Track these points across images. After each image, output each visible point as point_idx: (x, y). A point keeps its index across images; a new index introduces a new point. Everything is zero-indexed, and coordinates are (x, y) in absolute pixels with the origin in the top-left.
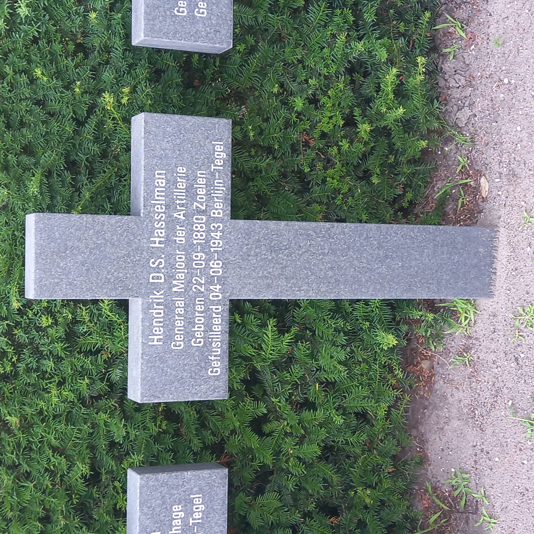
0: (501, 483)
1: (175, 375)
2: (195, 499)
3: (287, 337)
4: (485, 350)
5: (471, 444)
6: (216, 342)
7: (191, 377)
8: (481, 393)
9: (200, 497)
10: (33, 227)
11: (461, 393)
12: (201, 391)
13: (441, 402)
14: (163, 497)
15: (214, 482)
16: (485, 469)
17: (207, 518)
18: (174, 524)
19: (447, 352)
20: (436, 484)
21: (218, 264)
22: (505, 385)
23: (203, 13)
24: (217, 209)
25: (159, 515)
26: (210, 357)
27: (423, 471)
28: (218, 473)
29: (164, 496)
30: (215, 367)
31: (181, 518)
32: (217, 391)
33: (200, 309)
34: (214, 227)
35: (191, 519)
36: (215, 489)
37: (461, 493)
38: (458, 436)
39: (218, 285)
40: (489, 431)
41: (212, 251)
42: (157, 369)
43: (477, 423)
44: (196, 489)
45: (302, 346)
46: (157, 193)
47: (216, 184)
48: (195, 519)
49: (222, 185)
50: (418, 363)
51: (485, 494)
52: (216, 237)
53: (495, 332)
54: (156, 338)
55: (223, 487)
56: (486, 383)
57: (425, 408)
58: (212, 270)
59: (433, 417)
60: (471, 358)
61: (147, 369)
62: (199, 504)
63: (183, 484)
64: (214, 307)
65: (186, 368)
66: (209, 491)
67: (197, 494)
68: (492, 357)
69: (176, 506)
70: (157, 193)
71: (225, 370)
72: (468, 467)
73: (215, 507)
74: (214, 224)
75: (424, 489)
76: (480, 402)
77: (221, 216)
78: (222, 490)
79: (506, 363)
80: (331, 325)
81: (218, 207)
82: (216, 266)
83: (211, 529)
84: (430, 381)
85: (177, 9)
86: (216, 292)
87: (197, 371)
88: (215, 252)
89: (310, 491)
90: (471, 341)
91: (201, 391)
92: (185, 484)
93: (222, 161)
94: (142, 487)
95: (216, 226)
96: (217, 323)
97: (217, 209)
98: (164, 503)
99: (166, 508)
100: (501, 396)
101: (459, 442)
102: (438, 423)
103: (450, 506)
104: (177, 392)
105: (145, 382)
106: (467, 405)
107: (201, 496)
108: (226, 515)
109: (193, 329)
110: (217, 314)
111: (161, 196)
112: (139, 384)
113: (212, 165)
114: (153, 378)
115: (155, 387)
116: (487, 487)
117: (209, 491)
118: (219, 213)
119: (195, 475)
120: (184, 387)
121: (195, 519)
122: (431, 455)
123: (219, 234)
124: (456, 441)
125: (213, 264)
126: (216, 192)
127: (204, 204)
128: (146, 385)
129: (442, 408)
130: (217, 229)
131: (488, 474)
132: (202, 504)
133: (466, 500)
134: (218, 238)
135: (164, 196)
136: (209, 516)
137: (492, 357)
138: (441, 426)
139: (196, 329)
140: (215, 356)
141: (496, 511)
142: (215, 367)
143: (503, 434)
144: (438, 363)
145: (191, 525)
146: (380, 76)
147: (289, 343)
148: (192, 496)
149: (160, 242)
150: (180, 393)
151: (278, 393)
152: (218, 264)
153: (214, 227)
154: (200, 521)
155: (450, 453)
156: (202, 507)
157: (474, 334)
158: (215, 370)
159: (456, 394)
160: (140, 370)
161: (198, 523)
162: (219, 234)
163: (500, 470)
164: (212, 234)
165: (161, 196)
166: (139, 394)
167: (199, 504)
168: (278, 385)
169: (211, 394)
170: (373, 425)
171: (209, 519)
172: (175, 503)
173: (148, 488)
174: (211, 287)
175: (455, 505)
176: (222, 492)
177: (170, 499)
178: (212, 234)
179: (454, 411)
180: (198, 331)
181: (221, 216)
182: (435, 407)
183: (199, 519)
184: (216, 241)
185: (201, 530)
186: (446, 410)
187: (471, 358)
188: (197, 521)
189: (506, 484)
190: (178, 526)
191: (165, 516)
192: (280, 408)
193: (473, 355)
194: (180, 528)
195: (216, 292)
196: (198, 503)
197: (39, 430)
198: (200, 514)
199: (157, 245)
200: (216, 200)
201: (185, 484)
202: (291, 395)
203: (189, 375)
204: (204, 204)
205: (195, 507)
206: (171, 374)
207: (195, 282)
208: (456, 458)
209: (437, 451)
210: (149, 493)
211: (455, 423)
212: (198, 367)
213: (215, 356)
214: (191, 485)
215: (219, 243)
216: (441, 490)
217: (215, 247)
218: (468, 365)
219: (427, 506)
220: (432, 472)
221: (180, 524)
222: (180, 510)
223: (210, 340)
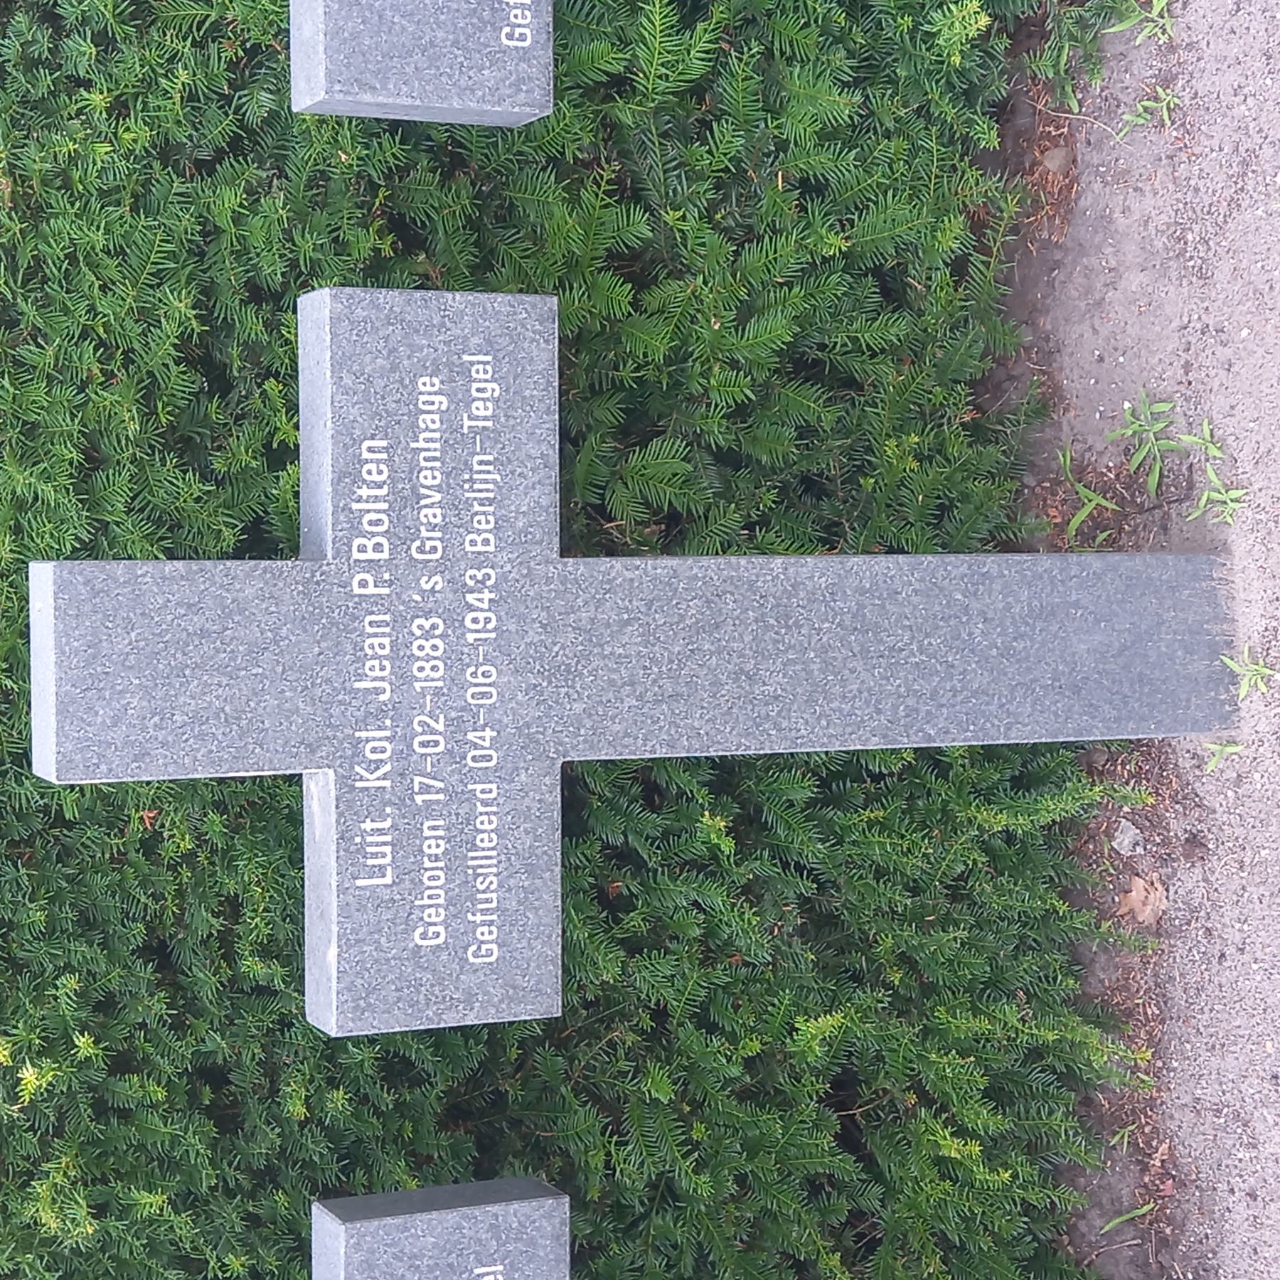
0: (1255, 394)
1: (413, 33)
2: (476, 367)
3: (701, 37)
4: (1211, 66)
5: (1176, 323)
6: (486, 875)
7: (455, 43)
8: (1201, 184)
9: (488, 363)
10: (50, 657)
11: (1149, 201)
12: (483, 86)
13: (1096, 232)
14: (390, 352)
15: (523, 326)
16: (1212, 373)
17: (507, 417)
18: (423, 426)
19: (1111, 106)
20: (1083, 456)
22: (1266, 138)
24: (479, 532)
25: (383, 398)
27: (1049, 433)
28: (534, 306)
29: (395, 350)
30: (519, 26)
31: (439, 411)
32: (524, 88)
33: (434, 851)
35: (465, 416)
36: (526, 345)
37: (1149, 461)
38: (1141, 314)
40: (1222, 273)
42: (367, 14)
43: (1191, 263)
44: (475, 340)
45: (741, 60)
48: (477, 418)
50: (1035, 163)
51: (1212, 436)
52: (477, 604)
53: (1238, 10)
55: (547, 341)
56: (1214, 154)
57: (1057, 265)
59: (1078, 279)
60: (1176, 100)
61: (340, 10)
62: (486, 381)
63: (443, 325)
64: (479, 787)
65: (443, 17)
66: (511, 348)
67: (480, 353)
68: (1233, 77)
69: (427, 379)
71: (545, 36)
72: (1167, 387)
73: (527, 393)
75: (1050, 480)
76: (1198, 209)
77: (491, 548)
78: (544, 350)
79: (1268, 82)
80: (815, 9)
81: (484, 526)
82: (481, 680)
83: (518, 448)
84: (1065, 203)
86: (483, 748)
87: (470, 29)
89: (764, 459)
90: (1173, 59)
91: (483, 86)
92: (448, 324)
94: (335, 320)
96: (486, 827)
97: (479, 532)
98: (394, 368)
99: (401, 381)
100: (1253, 172)
101: (1142, 328)
102: (1088, 291)
103: (1121, 502)
104: (420, 80)
105: (336, 43)
106: (1164, 227)
107: (489, 358)
108: (557, 417)
112: (321, 48)
114: (355, 36)
115: (361, 59)
116: (1218, 418)
117: (511, 348)
119: (474, 305)
120: (438, 68)
121: (477, 418)
122: (1073, 381)
123: (487, 595)
124: (1137, 327)
126: (476, 486)
128: (339, 51)
129: (1099, 249)
131: (1222, 384)
132: (494, 380)
133: (1161, 475)
136: (511, 413)
137: (1233, 77)
138: (1097, 297)
139: (426, 902)
141: (1240, 470)
142: (519, 26)
143: (1259, 265)
144: (1089, 143)
145: (465, 431)
147: (707, 52)
148: (466, 358)
150: (428, 83)
151: (679, 198)
154: (489, 424)
155: (1121, 359)
156: (494, 389)
157: (1184, 35)
158: (518, 31)
159: (1135, 206)
160: (321, 11)
161: (484, 428)
162: (487, 595)
163: (1252, 360)
164: (470, 598)
166: (322, 74)
167: (486, 381)
168: (679, 176)
169: (509, 97)
170: (921, 313)
171: (512, 422)
172: (423, 370)
173: (351, 323)
174: (471, 736)
175: (1133, 496)
176: (545, 356)
177: (409, 357)
178: (470, 598)
179: (1131, 251)
180: (430, 906)
182: (1082, 249)
183: (485, 418)
184: (481, 616)
185: (492, 448)
186: (1111, 249)
187: (1176, 100)
188: (481, 424)
189: (1269, 391)
190: (434, 431)
191: (398, 402)
192: (684, 238)
193: (1180, 94)
194: (437, 435)
195: (483, 748)
196: (481, 376)
197: (63, 225)
198: (489, 404)
200: (477, 508)
201: (448, 324)
202: (713, 207)
203: (451, 37)
205: (475, 385)
206: (404, 29)
208: (1136, 371)
209: (1086, 366)
210: (355, 338)
211: (1134, 281)
212: (475, 20)
214: (463, 330)
215: (488, 620)
216: (1095, 469)
217: (477, 631)
218: (1168, 123)
219: (1058, 520)
220: (1072, 429)
221: (437, 425)
222: (436, 389)
223: (470, 871)
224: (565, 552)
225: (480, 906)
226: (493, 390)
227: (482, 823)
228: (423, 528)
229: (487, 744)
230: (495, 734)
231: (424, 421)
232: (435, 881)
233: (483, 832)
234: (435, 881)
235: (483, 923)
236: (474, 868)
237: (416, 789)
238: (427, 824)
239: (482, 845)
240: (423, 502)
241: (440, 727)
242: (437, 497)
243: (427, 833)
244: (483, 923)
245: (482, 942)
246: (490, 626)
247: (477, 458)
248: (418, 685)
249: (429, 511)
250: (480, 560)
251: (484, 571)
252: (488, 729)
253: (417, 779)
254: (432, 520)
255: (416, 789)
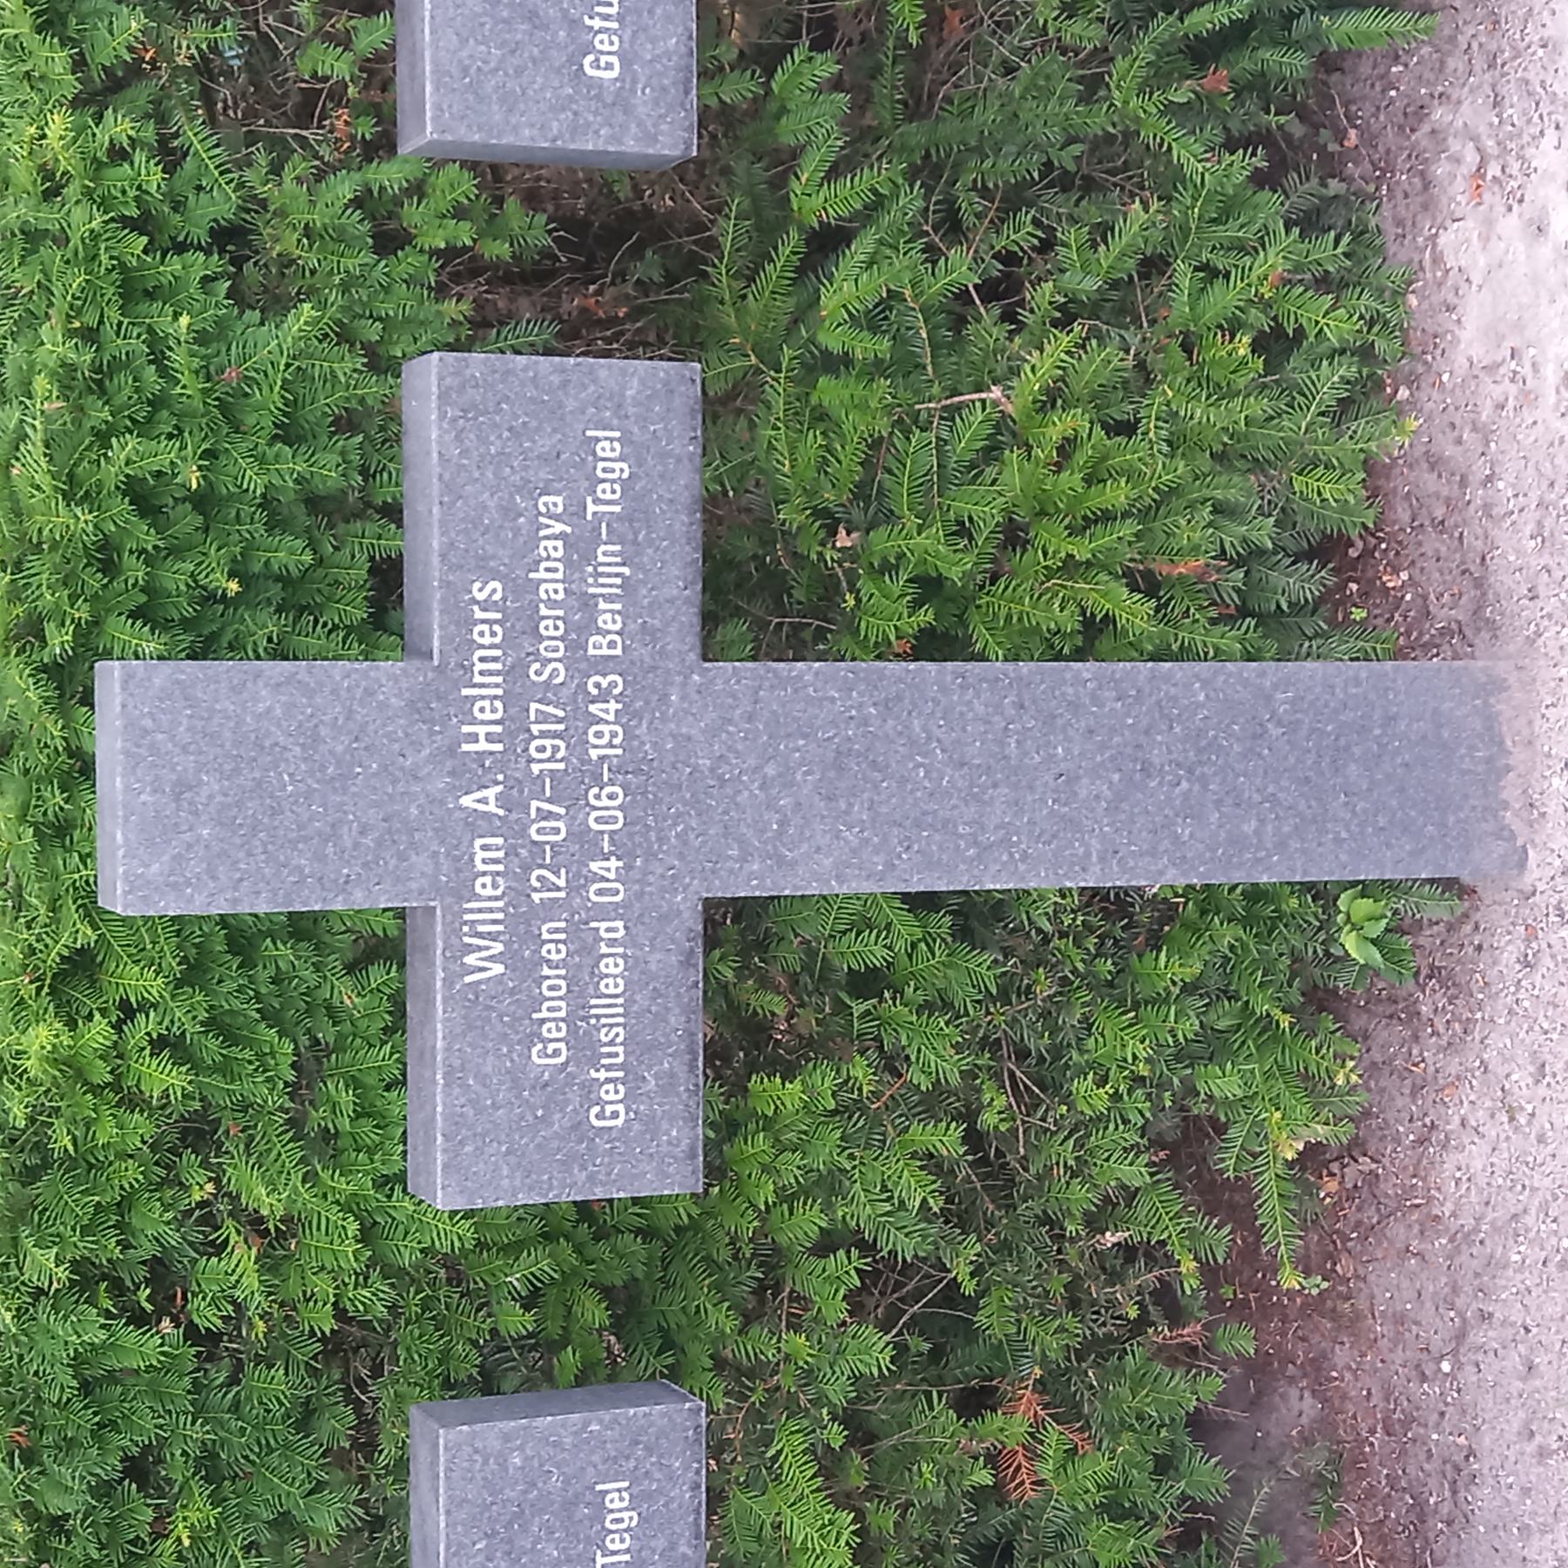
21: (611, 797)
23: (615, 1115)
26: (588, 22)
34: (598, 685)
39: (613, 858)
41: (594, 757)
46: (479, 666)
47: (601, 559)
48: (614, 1553)
49: (618, 560)
54: (482, 730)
58: (595, 814)
62: (546, 581)
64: (603, 925)
70: (479, 666)
74: (597, 678)
77: (618, 651)
81: (610, 626)
82: (605, 802)
85: (596, 1109)
86: (608, 880)
88: (602, 758)
93: (617, 487)
95: (604, 685)
96: (612, 970)
109: (532, 575)
110: (612, 943)
111: (491, 673)
113: (589, 500)
118: (612, 645)
123: (613, 706)
125: (598, 797)
126: (601, 580)
127: (533, 814)
130: (604, 696)
132: (621, 459)
134: (611, 718)
135: (498, 673)
139: (544, 1014)
140: (609, 1068)
146: (179, 1094)
149: (490, 738)
152: (611, 797)
153: (598, 685)
156: (623, 469)
162: (613, 706)
164: (593, 708)
165: (491, 673)
174: (594, 866)
178: (593, 708)
181: (618, 651)
184: (605, 728)
195: (608, 880)
199: (483, 746)
200: (602, 605)
204: (533, 814)
207: (537, 885)
213: (609, 1068)
215: (614, 735)
224: (708, 904)
225: (604, 1061)
226: (622, 470)
227: (602, 42)
228: (542, 606)
229: (612, 876)
230: (620, 706)
231: (546, 549)
232: (554, 982)
233: (607, 976)
234: (554, 982)
235: (608, 1081)
236: (598, 1017)
237: (532, 718)
238: (544, 928)
239: (606, 991)
240: (542, 533)
241: (562, 883)
242: (559, 527)
243: (545, 936)
244: (608, 1081)
245: (602, 53)
246: (616, 741)
247: (603, 548)
248: (536, 768)
249: (550, 544)
250: (603, 665)
251: (611, 678)
252: (613, 858)
253: (534, 706)
254: (553, 596)
255: (532, 718)
